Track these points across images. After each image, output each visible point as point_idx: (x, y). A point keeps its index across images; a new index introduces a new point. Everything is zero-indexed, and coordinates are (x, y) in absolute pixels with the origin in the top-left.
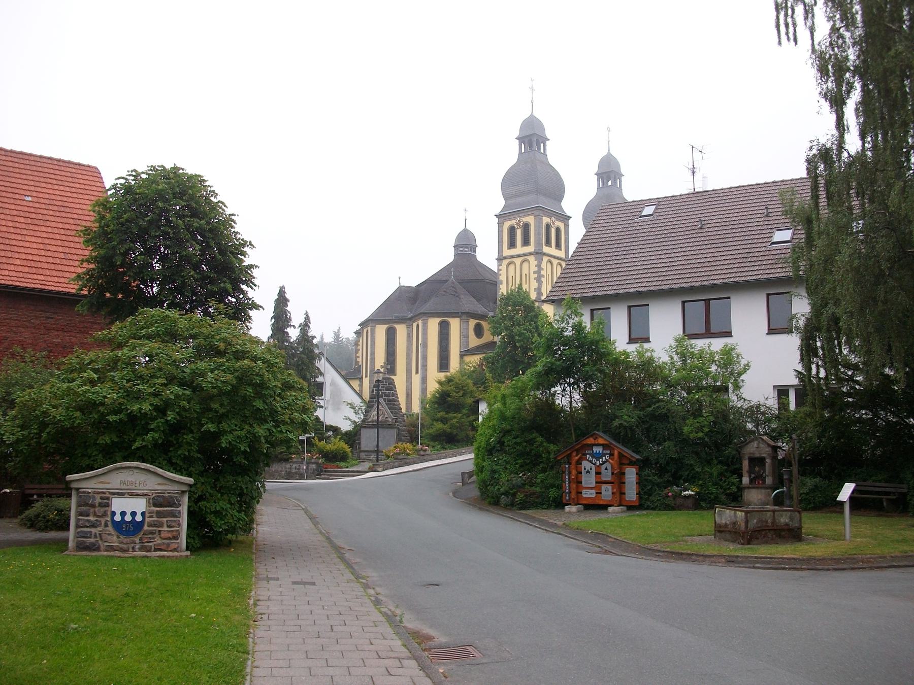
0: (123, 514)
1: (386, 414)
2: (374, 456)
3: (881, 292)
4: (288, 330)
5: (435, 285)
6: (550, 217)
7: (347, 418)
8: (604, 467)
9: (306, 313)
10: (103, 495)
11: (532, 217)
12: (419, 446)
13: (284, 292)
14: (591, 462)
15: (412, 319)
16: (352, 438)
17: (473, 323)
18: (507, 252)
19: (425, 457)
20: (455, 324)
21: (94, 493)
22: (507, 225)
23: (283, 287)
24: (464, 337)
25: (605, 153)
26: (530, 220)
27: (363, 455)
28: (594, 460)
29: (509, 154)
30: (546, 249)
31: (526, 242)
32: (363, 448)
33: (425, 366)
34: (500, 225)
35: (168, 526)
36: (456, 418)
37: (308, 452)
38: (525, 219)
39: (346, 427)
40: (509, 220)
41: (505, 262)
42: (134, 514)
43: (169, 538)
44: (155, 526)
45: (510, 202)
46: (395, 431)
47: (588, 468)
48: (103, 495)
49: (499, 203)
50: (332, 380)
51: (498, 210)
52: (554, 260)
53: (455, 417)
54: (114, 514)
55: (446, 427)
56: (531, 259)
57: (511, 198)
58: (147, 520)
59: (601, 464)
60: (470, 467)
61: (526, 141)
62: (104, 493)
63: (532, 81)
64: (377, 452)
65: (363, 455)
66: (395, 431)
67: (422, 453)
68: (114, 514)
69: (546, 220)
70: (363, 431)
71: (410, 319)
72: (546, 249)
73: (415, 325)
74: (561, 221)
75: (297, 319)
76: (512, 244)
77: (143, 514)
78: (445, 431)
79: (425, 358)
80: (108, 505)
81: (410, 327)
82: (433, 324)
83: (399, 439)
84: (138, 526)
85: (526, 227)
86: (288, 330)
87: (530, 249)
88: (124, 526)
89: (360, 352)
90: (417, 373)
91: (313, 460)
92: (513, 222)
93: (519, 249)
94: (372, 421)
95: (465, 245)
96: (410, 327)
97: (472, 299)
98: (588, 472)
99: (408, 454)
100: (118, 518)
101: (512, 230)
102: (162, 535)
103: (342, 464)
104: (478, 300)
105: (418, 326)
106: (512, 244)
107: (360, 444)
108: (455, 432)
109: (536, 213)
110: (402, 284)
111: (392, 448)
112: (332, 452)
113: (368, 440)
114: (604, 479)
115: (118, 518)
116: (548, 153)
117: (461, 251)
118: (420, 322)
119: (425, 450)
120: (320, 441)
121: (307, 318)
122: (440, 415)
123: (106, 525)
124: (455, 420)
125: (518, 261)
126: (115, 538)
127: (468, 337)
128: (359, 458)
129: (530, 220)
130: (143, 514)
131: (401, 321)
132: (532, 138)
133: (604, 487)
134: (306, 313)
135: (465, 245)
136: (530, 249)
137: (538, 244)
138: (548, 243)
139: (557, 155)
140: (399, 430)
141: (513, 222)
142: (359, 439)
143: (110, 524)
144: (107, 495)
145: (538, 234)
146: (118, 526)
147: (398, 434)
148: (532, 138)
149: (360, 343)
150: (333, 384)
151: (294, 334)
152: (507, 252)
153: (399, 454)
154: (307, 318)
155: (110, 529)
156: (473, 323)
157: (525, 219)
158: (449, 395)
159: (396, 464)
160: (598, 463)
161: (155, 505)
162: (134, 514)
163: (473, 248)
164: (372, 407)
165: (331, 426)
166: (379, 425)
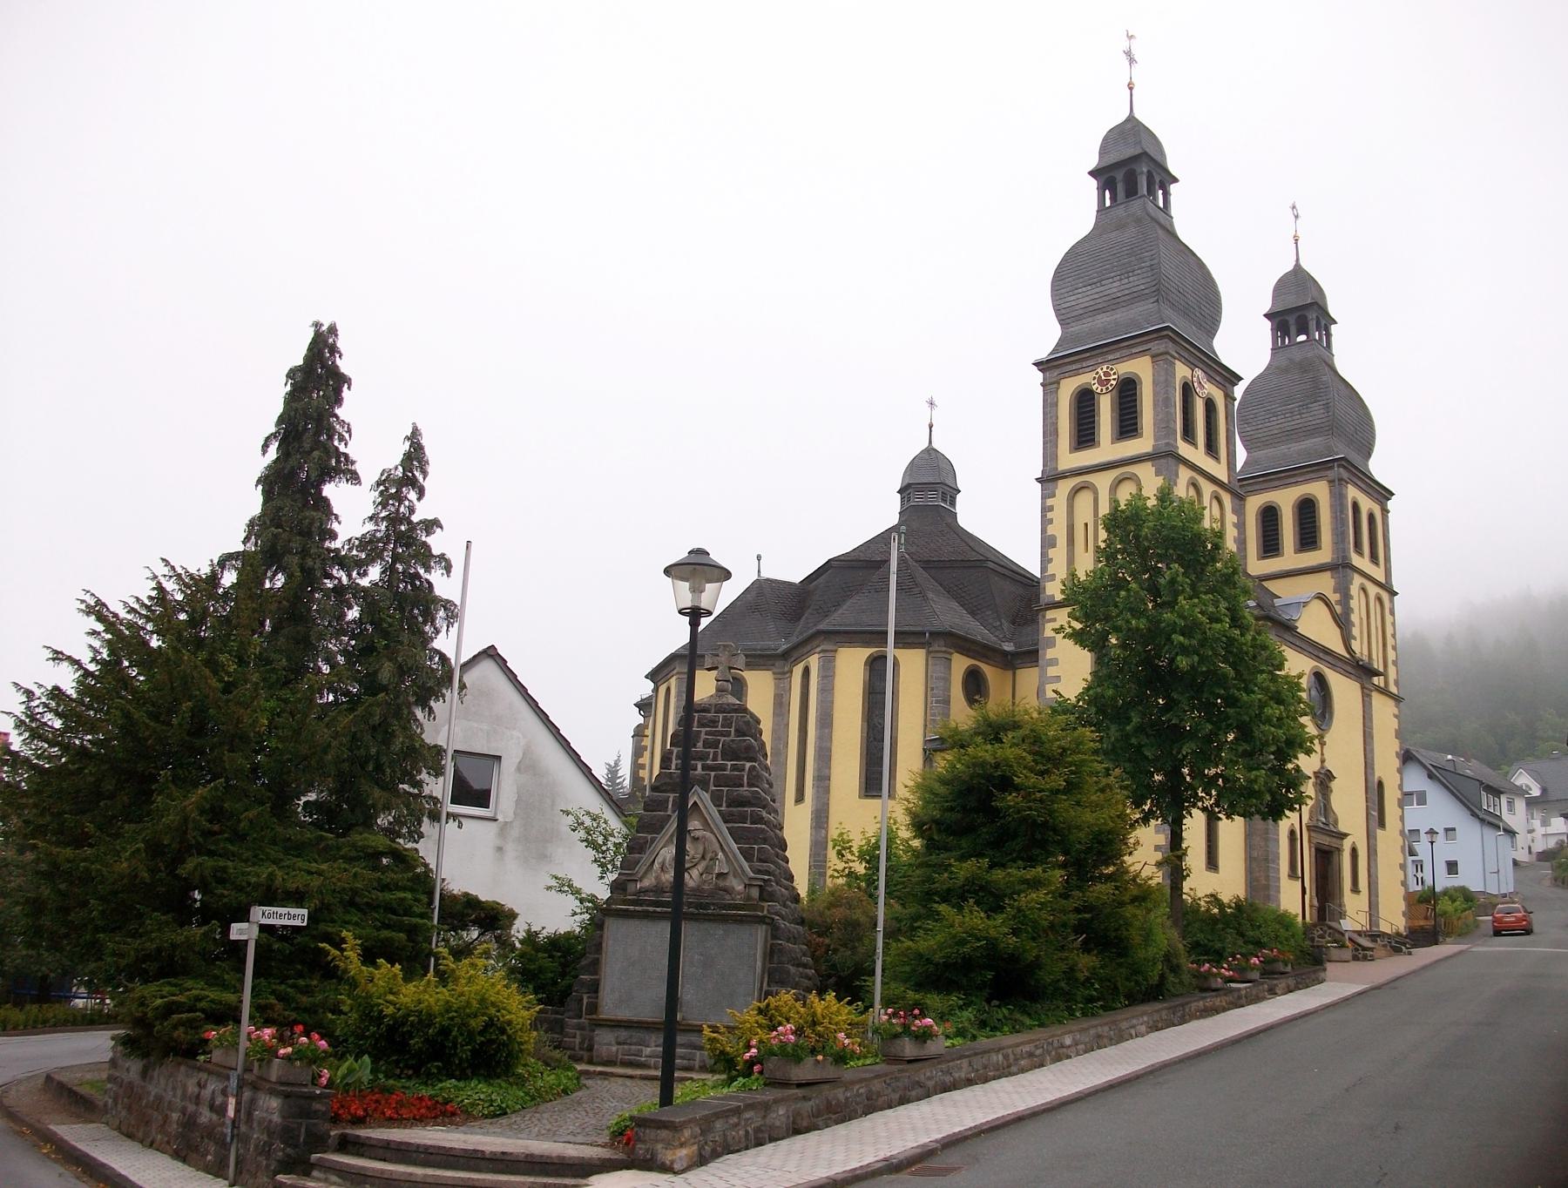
1: (716, 855)
2: (652, 1048)
3: (388, 1113)
4: (332, 491)
5: (852, 573)
6: (1192, 366)
7: (565, 886)
9: (414, 438)
12: (879, 1015)
13: (334, 350)
15: (789, 657)
16: (559, 970)
17: (960, 664)
18: (1069, 460)
19: (927, 1074)
20: (911, 667)
22: (1069, 387)
23: (333, 330)
24: (936, 700)
25: (1290, 267)
26: (1141, 368)
27: (606, 1042)
29: (1076, 210)
30: (1184, 449)
31: (1127, 426)
32: (611, 1003)
33: (823, 780)
34: (1050, 388)
36: (1041, 888)
37: (263, 1016)
38: (1125, 368)
39: (547, 913)
40: (1076, 373)
41: (1064, 487)
45: (1076, 328)
46: (760, 933)
49: (1046, 335)
50: (527, 752)
51: (1044, 353)
52: (1202, 482)
53: (1035, 884)
55: (997, 926)
56: (1146, 472)
57: (1078, 318)
61: (1119, 175)
63: (1130, 37)
64: (670, 1027)
65: (606, 1042)
66: (760, 933)
67: (909, 1048)
69: (1182, 371)
70: (615, 930)
71: (785, 656)
73: (798, 671)
74: (1219, 385)
75: (371, 443)
76: (1085, 436)
78: (992, 944)
79: (824, 756)
81: (783, 677)
82: (851, 663)
83: (775, 977)
86: (332, 491)
87: (1142, 445)
89: (647, 754)
90: (800, 798)
91: (276, 1070)
92: (1086, 379)
93: (1108, 448)
94: (658, 889)
95: (929, 487)
96: (783, 677)
97: (955, 605)
99: (841, 1058)
101: (1085, 401)
103: (476, 1091)
104: (973, 614)
105: (806, 671)
106: (1085, 436)
107: (594, 988)
108: (1032, 950)
109: (1157, 347)
110: (765, 574)
111: (749, 1016)
112: (426, 1019)
113: (630, 976)
116: (1174, 211)
117: (917, 500)
118: (814, 661)
119: (924, 1036)
120: (369, 957)
121: (415, 456)
122: (965, 869)
124: (1040, 895)
125: (1103, 481)
127: (947, 702)
128: (588, 1053)
129: (1141, 368)
131: (758, 660)
132: (1132, 171)
134: (414, 438)
135: (929, 487)
136: (1142, 445)
137: (1164, 427)
138: (1189, 434)
139: (1194, 215)
140: (775, 932)
141: (1086, 379)
142: (595, 966)
145: (1163, 402)
147: (771, 953)
148: (1132, 171)
149: (648, 732)
150: (529, 765)
151: (352, 510)
152: (1069, 460)
153: (794, 1056)
154: (415, 456)
156: (960, 664)
157: (1125, 368)
158: (1006, 784)
159: (780, 1115)
163: (951, 493)
164: (655, 827)
165: (471, 902)
166: (678, 908)
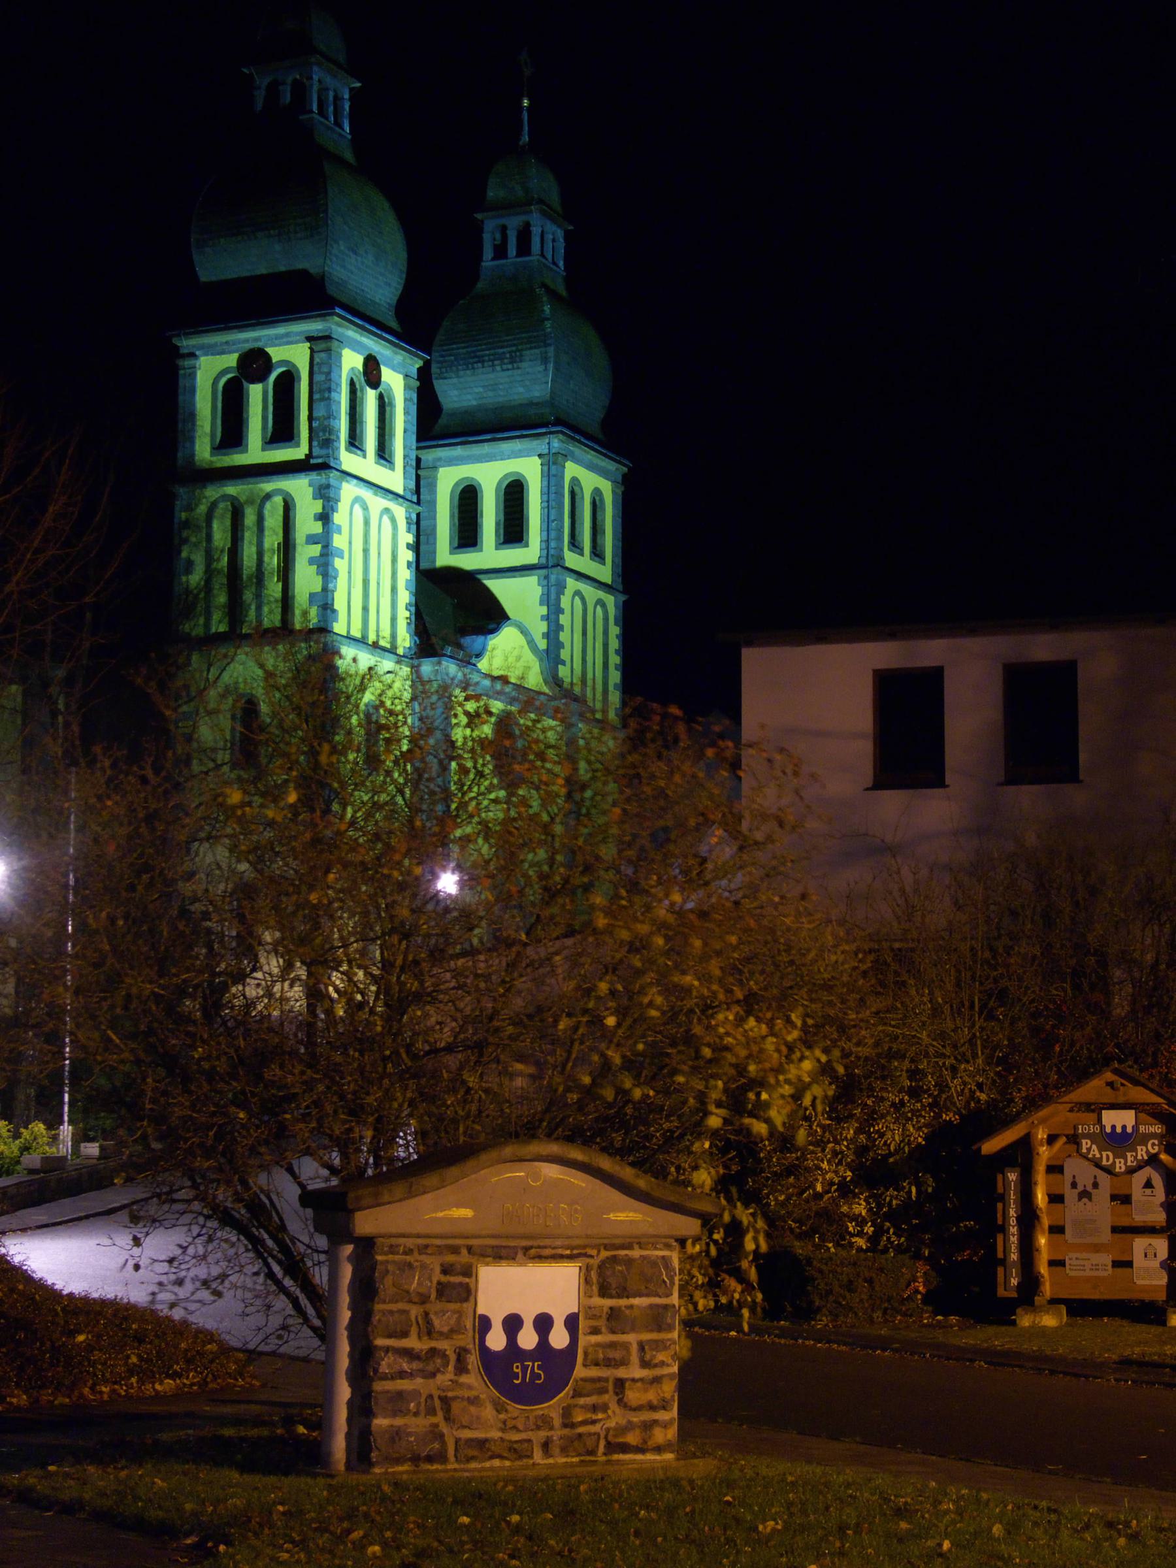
0: (513, 1324)
8: (1139, 1178)
10: (450, 1258)
11: (536, 462)
14: (1097, 1164)
21: (423, 1249)
28: (1107, 1158)
35: (645, 1364)
42: (543, 1323)
43: (652, 1407)
44: (609, 1363)
47: (1085, 1182)
48: (450, 1258)
54: (485, 1324)
58: (584, 1340)
59: (1131, 1171)
60: (358, 1216)
62: (455, 1250)
68: (485, 1324)
72: (571, 559)
77: (571, 1323)
80: (467, 1293)
84: (555, 1365)
85: (514, 493)
87: (530, 553)
88: (517, 1368)
98: (1085, 1195)
100: (496, 1340)
102: (633, 1396)
114: (1139, 1219)
115: (496, 1340)
123: (461, 1368)
126: (488, 1412)
130: (571, 1323)
133: (1140, 1244)
136: (530, 553)
143: (473, 1360)
144: (464, 1258)
146: (499, 1367)
155: (474, 1380)
160: (1120, 1166)
161: (604, 1292)
162: (543, 1323)
